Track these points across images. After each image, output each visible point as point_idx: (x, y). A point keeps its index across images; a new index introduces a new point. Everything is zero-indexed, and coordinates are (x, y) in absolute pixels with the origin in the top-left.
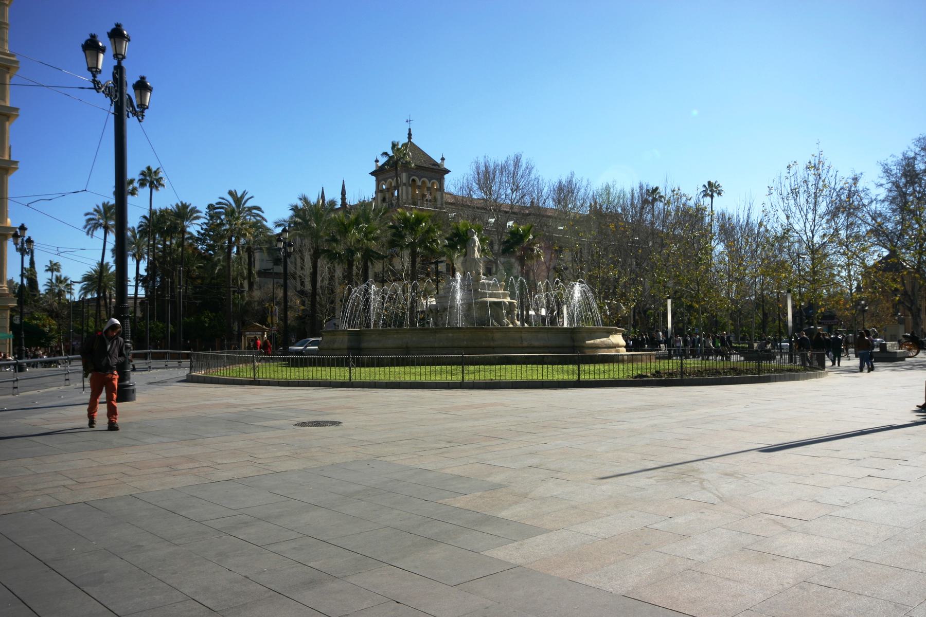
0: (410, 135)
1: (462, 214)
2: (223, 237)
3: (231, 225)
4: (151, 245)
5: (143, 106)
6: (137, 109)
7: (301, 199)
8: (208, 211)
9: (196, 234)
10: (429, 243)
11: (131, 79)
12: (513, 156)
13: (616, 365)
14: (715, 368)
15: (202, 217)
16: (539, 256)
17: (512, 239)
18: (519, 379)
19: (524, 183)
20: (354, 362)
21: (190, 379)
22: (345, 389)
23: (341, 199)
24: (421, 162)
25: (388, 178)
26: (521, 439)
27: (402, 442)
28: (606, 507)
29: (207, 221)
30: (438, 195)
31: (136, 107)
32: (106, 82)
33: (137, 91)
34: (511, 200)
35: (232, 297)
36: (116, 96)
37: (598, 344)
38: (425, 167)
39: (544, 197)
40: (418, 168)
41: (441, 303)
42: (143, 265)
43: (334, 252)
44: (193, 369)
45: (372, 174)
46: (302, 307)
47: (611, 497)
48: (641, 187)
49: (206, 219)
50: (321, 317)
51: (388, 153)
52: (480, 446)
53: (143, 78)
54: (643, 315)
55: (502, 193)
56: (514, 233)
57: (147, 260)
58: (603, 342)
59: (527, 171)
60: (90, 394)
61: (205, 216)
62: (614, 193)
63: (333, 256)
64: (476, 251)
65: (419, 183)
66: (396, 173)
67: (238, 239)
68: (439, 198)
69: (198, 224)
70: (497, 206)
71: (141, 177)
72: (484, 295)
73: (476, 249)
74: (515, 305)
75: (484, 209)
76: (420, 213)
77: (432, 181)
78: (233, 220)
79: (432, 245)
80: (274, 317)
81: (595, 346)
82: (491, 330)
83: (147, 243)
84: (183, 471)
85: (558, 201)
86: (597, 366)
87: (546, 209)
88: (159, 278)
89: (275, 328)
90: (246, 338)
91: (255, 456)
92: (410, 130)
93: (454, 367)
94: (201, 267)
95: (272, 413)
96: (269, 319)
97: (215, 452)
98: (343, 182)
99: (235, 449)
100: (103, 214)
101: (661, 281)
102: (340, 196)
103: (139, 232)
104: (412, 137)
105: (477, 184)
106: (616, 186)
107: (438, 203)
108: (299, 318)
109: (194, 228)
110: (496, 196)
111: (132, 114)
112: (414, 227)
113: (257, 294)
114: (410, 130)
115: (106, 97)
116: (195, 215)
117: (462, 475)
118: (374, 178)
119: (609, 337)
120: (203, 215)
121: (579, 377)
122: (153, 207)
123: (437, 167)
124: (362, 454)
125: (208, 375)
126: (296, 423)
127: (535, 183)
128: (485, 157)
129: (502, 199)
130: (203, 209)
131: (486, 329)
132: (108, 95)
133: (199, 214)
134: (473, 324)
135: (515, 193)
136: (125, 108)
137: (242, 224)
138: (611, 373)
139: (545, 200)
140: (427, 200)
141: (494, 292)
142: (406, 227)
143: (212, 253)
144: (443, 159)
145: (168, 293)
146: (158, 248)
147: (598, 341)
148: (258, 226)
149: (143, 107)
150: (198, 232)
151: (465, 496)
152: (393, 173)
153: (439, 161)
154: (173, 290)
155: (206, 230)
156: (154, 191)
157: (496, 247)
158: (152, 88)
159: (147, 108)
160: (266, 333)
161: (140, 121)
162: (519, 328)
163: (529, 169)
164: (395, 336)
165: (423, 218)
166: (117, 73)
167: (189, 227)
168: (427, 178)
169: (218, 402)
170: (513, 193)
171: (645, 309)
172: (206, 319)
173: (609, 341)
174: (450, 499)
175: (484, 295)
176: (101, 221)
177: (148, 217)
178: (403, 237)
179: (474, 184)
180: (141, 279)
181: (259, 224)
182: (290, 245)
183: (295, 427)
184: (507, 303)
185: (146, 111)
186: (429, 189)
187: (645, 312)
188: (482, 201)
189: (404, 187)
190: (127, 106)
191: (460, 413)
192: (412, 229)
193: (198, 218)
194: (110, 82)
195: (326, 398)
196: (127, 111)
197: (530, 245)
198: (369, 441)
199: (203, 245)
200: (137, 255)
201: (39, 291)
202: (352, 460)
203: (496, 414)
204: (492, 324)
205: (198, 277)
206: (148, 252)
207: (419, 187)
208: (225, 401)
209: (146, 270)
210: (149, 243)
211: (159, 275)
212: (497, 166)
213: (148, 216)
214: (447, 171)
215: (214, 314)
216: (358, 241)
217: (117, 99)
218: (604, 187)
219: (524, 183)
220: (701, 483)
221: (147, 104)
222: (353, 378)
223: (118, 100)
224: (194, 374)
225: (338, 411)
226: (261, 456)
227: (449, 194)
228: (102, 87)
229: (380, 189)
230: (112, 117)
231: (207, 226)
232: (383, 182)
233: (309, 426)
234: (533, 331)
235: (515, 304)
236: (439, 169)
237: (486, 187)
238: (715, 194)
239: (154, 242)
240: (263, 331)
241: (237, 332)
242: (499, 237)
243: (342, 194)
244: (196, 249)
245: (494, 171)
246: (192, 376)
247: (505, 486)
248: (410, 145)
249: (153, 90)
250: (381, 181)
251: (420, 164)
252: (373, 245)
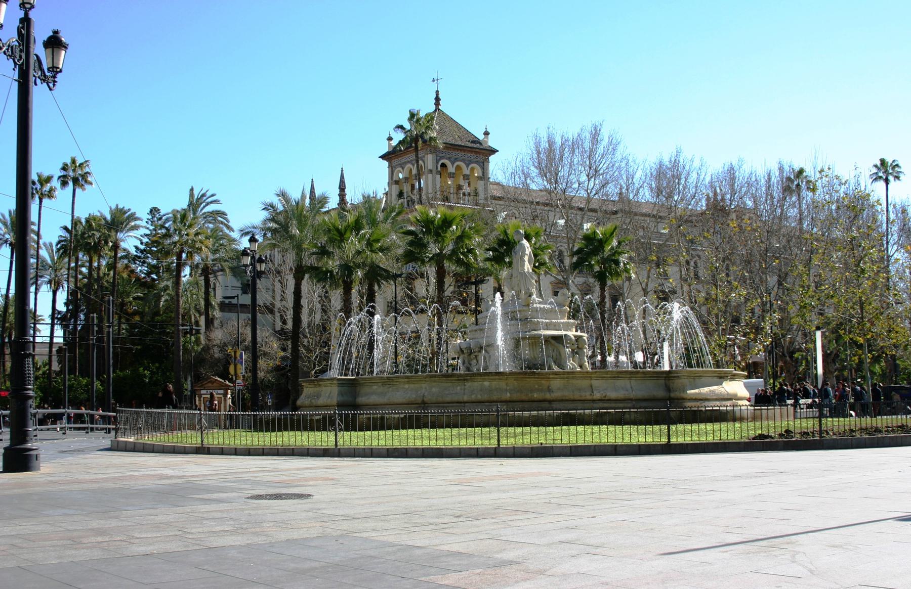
0: (437, 99)
1: (516, 212)
2: (168, 253)
3: (181, 236)
4: (72, 268)
5: (55, 70)
6: (47, 74)
7: (278, 195)
8: (150, 217)
9: (133, 251)
10: (463, 254)
11: (40, 34)
12: (590, 125)
13: (730, 424)
14: (875, 425)
15: (142, 227)
16: (627, 271)
17: (587, 246)
18: (581, 442)
19: (605, 166)
20: (341, 420)
21: (116, 447)
22: (329, 458)
23: (339, 195)
24: (454, 138)
25: (406, 163)
26: (560, 513)
27: (391, 517)
28: (648, 584)
29: (148, 232)
30: (480, 185)
31: (46, 71)
32: (9, 40)
33: (47, 50)
34: (587, 191)
35: (182, 339)
36: (21, 57)
37: (704, 394)
38: (461, 146)
39: (637, 185)
40: (450, 147)
41: (475, 338)
42: (62, 296)
43: (324, 269)
44: (119, 434)
45: (383, 157)
46: (282, 354)
47: (661, 572)
48: (781, 169)
49: (148, 228)
50: (307, 367)
51: (404, 126)
52: (499, 521)
53: (56, 32)
54: (788, 358)
55: (574, 181)
56: (590, 239)
57: (66, 289)
58: (713, 391)
59: (610, 148)
61: (145, 224)
62: (741, 178)
63: (321, 275)
64: (527, 263)
65: (451, 169)
66: (417, 156)
67: (190, 255)
68: (481, 190)
69: (135, 237)
70: (566, 199)
71: (63, 173)
72: (536, 327)
73: (526, 258)
74: (584, 340)
75: (547, 205)
76: (448, 212)
77: (471, 166)
78: (183, 229)
79: (467, 257)
80: (239, 366)
81: (700, 397)
82: (546, 377)
83: (67, 266)
84: (89, 545)
85: (659, 192)
86: (702, 426)
87: (639, 204)
88: (83, 314)
89: (240, 381)
90: (202, 399)
91: (186, 530)
93: (486, 430)
94: (139, 298)
95: (220, 485)
96: (232, 369)
97: (133, 526)
98: (342, 177)
99: (160, 523)
100: (10, 226)
101: (807, 305)
102: (338, 191)
103: (58, 250)
104: (441, 102)
105: (536, 167)
106: (743, 167)
107: (480, 198)
108: (277, 369)
109: (130, 242)
110: (564, 184)
111: (41, 80)
112: (440, 231)
113: (218, 335)
114: (437, 92)
115: (8, 59)
116: (133, 224)
117: (463, 551)
118: (386, 163)
119: (721, 384)
120: (143, 223)
121: (669, 438)
122: (76, 214)
123: (478, 145)
124: (331, 530)
125: (140, 441)
126: (250, 495)
127: (623, 164)
128: (549, 128)
129: (574, 189)
130: (143, 214)
131: (538, 374)
132: (10, 56)
133: (138, 222)
134: (522, 369)
135: (593, 179)
136: (32, 72)
137: (197, 234)
138: (717, 433)
139: (638, 190)
140: (464, 194)
141: (553, 321)
142: (428, 232)
143: (155, 277)
144: (486, 133)
145: (93, 335)
146: (81, 273)
147: (705, 390)
148: (219, 238)
149: (55, 70)
150: (136, 247)
151: (460, 573)
152: (412, 156)
153: (481, 137)
154: (100, 331)
155: (147, 244)
156: (78, 191)
157: (567, 262)
158: (68, 45)
159: (61, 71)
160: (229, 391)
161: (51, 89)
162: (588, 372)
163: (613, 146)
164: (407, 386)
165: (454, 219)
166: (23, 28)
167: (124, 241)
168: (462, 161)
169: (147, 473)
170: (589, 180)
171: (791, 349)
172: (146, 372)
173: (723, 390)
174: (436, 576)
175: (536, 327)
176: (7, 236)
177: (70, 228)
178: (423, 246)
179: (532, 168)
180: (59, 316)
181: (221, 233)
182: (260, 261)
183: (247, 500)
184: (573, 337)
185: (59, 76)
186: (466, 177)
187: (791, 354)
188: (545, 193)
189: (430, 175)
190: (34, 70)
191: (483, 484)
192: (438, 235)
193: (136, 228)
194: (14, 40)
195: (298, 469)
196: (34, 76)
197: (613, 255)
198: (345, 516)
199: (142, 266)
200: (53, 282)
202: (315, 536)
203: (535, 485)
204: (550, 368)
205: (135, 313)
206: (68, 278)
207: (451, 176)
208: (160, 472)
209: (66, 304)
210: (69, 265)
211: (82, 311)
212: (566, 141)
214: (493, 151)
215: (157, 365)
216: (359, 253)
217: (21, 61)
218: (726, 169)
219: (605, 166)
220: (793, 556)
221: (60, 67)
222: (340, 442)
223: (23, 63)
224: (121, 439)
225: (311, 483)
226: (193, 531)
227: (498, 184)
228: (3, 46)
230: (15, 85)
231: (148, 238)
232: (400, 169)
233: (266, 499)
234: (609, 376)
235: (585, 338)
236: (481, 147)
237: (550, 172)
238: (891, 178)
239: (77, 262)
240: (226, 388)
241: (190, 391)
242: (571, 245)
243: (340, 188)
244: (132, 271)
245: (562, 149)
246: (118, 441)
247: (519, 563)
249: (69, 47)
250: (396, 168)
251: (453, 142)
252: (381, 260)
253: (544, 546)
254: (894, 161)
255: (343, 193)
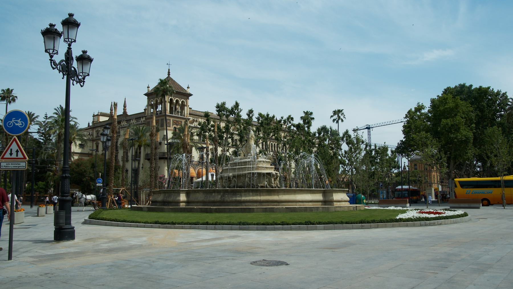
0: (169, 73)
45: (145, 95)
60: (54, 223)
92: (169, 70)
98: (125, 102)
102: (123, 108)
118: (146, 97)
144: (188, 88)
153: (186, 89)
201: (253, 119)
213: (270, 116)
229: (150, 104)
248: (169, 79)
253: (416, 286)
254: (16, 97)
255: (125, 108)
